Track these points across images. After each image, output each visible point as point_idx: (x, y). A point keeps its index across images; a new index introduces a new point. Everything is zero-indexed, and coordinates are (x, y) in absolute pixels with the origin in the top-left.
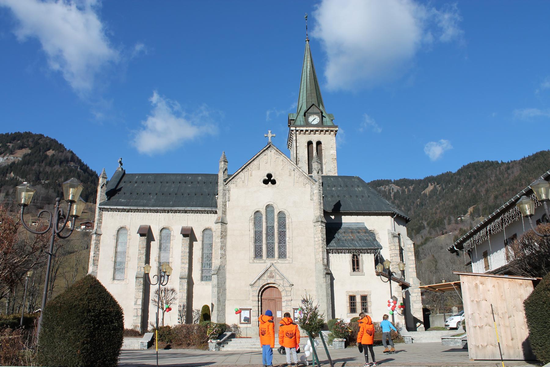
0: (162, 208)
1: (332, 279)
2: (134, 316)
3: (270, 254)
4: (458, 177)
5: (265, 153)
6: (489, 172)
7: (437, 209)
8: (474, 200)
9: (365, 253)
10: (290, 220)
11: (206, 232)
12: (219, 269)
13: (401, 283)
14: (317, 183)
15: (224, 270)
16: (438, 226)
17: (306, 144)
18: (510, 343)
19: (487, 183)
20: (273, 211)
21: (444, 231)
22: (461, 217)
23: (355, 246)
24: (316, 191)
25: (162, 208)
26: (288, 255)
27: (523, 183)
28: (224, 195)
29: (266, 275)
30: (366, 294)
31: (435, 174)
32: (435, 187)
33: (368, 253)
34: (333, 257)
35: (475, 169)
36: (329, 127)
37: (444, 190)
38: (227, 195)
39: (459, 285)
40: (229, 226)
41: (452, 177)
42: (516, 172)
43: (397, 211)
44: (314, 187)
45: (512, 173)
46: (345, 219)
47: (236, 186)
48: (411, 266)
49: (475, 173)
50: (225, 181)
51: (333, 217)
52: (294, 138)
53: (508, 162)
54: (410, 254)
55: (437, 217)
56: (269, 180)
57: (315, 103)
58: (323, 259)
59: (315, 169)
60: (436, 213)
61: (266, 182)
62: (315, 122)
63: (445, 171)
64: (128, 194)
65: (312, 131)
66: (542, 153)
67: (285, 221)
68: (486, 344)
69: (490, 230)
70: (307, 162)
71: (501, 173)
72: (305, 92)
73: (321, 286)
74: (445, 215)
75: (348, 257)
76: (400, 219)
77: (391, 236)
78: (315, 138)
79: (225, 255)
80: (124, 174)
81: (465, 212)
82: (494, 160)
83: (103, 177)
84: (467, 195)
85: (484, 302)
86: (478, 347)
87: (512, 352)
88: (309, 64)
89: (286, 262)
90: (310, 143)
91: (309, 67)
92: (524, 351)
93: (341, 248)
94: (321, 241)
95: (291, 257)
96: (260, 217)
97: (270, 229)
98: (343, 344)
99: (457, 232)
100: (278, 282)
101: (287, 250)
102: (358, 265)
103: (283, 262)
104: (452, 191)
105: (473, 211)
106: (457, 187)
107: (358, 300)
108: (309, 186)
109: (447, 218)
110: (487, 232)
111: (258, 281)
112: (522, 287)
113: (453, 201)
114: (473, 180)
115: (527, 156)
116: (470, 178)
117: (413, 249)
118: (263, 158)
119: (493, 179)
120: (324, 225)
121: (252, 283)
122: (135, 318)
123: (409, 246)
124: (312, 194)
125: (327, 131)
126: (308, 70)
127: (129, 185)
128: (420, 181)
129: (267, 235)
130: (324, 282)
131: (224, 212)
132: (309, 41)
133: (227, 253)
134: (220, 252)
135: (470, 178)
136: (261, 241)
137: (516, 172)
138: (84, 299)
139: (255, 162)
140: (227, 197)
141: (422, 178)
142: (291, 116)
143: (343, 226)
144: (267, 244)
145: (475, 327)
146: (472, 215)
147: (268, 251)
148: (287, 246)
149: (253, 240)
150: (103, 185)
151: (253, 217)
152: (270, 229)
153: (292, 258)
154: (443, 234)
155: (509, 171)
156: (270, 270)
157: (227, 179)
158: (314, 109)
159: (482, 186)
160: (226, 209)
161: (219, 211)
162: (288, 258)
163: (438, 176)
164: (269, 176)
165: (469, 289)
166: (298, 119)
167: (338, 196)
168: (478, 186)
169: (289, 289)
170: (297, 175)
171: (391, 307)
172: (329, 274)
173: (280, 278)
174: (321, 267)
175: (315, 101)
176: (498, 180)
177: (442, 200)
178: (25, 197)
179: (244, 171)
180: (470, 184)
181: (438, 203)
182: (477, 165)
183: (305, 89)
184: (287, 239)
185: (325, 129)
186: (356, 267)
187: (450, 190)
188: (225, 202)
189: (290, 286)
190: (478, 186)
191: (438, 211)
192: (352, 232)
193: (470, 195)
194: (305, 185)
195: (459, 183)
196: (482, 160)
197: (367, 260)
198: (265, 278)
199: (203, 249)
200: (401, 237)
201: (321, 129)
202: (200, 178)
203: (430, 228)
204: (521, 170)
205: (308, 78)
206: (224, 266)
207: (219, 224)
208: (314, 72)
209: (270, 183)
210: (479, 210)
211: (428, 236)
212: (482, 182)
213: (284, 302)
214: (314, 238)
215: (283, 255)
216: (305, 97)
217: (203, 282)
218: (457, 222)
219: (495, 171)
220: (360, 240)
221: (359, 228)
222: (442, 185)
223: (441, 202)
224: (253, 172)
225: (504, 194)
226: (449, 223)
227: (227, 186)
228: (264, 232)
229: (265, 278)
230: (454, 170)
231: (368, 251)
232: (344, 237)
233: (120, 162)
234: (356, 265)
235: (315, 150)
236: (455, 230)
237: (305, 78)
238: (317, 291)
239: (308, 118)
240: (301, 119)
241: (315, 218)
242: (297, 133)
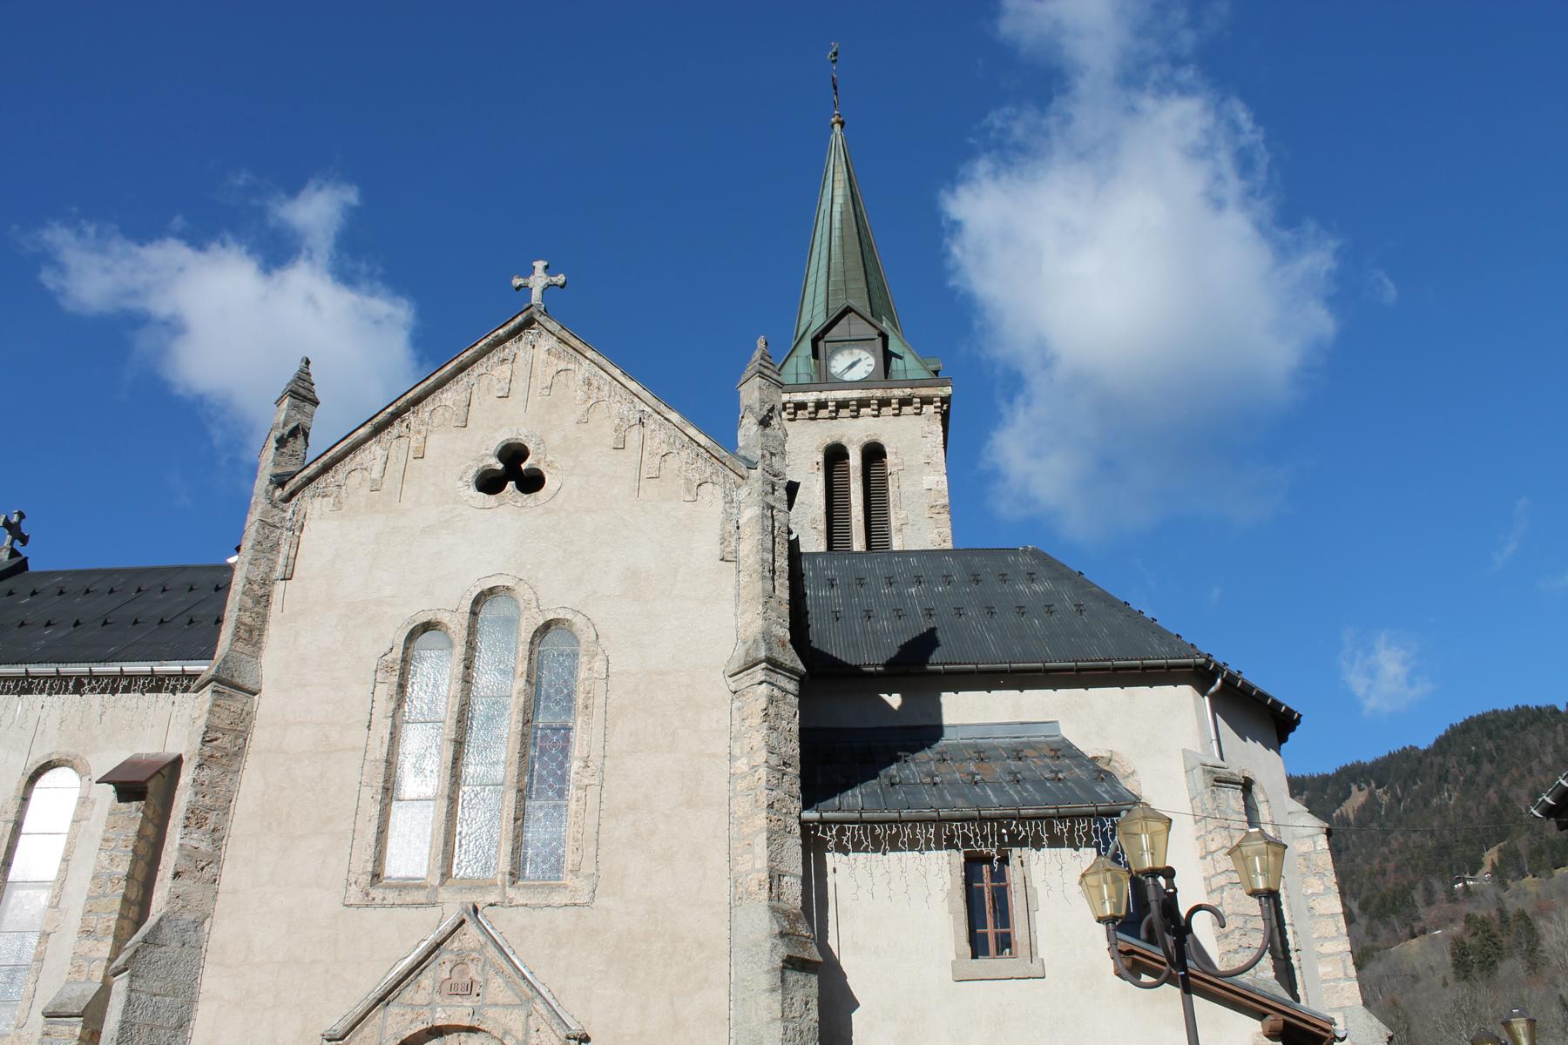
4: (1439, 759)
5: (498, 354)
6: (1533, 740)
7: (1386, 860)
8: (1500, 825)
9: (1037, 845)
10: (599, 665)
13: (1276, 1020)
14: (756, 474)
16: (1394, 911)
17: (820, 458)
19: (1530, 772)
21: (1417, 926)
29: (426, 980)
31: (1367, 758)
32: (1371, 794)
33: (1056, 842)
34: (847, 873)
35: (1490, 735)
36: (913, 384)
37: (1399, 801)
38: (284, 549)
40: (265, 706)
41: (1420, 761)
46: (963, 710)
47: (338, 504)
48: (1329, 947)
49: (1489, 745)
50: (280, 481)
51: (895, 700)
54: (1315, 885)
55: (1390, 885)
57: (853, 303)
58: (775, 877)
59: (750, 408)
60: (1383, 872)
61: (489, 483)
63: (1396, 747)
65: (842, 405)
70: (822, 526)
74: (1411, 876)
75: (935, 874)
77: (1200, 780)
78: (854, 433)
81: (1475, 866)
82: (1542, 704)
84: (1473, 814)
89: (557, 899)
90: (835, 456)
91: (839, 200)
94: (763, 772)
95: (588, 868)
99: (1457, 929)
104: (1426, 803)
105: (1500, 860)
106: (1439, 791)
108: (718, 491)
109: (1420, 886)
111: (378, 1016)
113: (1432, 833)
114: (1487, 768)
116: (1475, 760)
117: (1326, 860)
118: (491, 375)
119: (1549, 760)
120: (792, 686)
121: (340, 1028)
123: (1305, 846)
125: (904, 402)
126: (837, 208)
128: (1325, 779)
132: (842, 124)
135: (1475, 760)
140: (281, 560)
141: (1330, 771)
153: (595, 877)
154: (1414, 936)
156: (454, 945)
160: (264, 619)
162: (568, 880)
163: (1376, 763)
167: (929, 613)
168: (1506, 782)
173: (507, 996)
174: (759, 924)
177: (1397, 834)
179: (384, 436)
180: (1479, 779)
181: (1385, 842)
182: (1493, 721)
184: (575, 766)
185: (898, 393)
188: (266, 582)
190: (1506, 782)
191: (1390, 866)
193: (1483, 809)
195: (1443, 778)
196: (1506, 704)
200: (1259, 796)
203: (1372, 918)
206: (198, 924)
208: (858, 216)
209: (511, 485)
211: (1368, 943)
212: (1514, 771)
214: (732, 758)
218: (1452, 897)
219: (1551, 735)
222: (1391, 788)
223: (1396, 840)
224: (433, 440)
226: (1429, 902)
230: (1425, 742)
231: (1058, 828)
234: (988, 925)
236: (1452, 921)
239: (828, 359)
241: (741, 651)
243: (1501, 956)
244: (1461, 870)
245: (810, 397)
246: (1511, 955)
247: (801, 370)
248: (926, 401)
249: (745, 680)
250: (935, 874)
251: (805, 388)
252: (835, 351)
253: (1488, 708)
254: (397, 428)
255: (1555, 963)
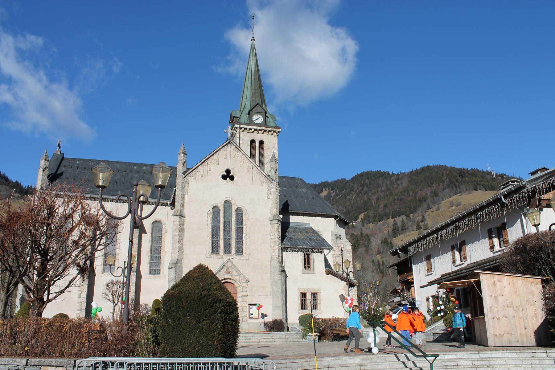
0: (111, 197)
1: (286, 276)
2: (78, 310)
3: (227, 250)
4: (352, 184)
6: (381, 182)
8: (365, 207)
11: (156, 225)
12: (177, 263)
14: (274, 182)
15: (181, 264)
17: (249, 143)
18: (524, 332)
19: (378, 192)
20: (230, 207)
22: (353, 223)
23: (308, 245)
24: (273, 190)
25: (111, 197)
26: (244, 251)
27: (411, 194)
28: (183, 188)
29: (222, 271)
30: (316, 291)
31: (330, 180)
32: (329, 192)
33: (319, 252)
35: (368, 178)
36: (272, 127)
39: (478, 283)
40: (187, 219)
41: (346, 184)
42: (405, 183)
43: (338, 213)
44: (271, 185)
45: (401, 184)
47: (195, 179)
49: (367, 182)
50: (184, 173)
52: (238, 135)
53: (398, 174)
54: (348, 255)
56: (228, 176)
58: (279, 256)
61: (224, 177)
62: (259, 122)
63: (339, 178)
64: (71, 179)
66: (428, 168)
67: (242, 217)
68: (503, 333)
69: (441, 236)
71: (391, 183)
72: (249, 90)
73: (276, 283)
75: (300, 256)
76: (342, 223)
78: (258, 137)
79: (182, 249)
80: (63, 158)
81: (356, 219)
82: (385, 171)
83: (45, 160)
84: (359, 202)
85: (501, 297)
86: (496, 335)
87: (525, 340)
88: (254, 63)
89: (243, 258)
90: (253, 142)
91: (254, 66)
92: (535, 338)
93: (295, 247)
94: (277, 239)
95: (248, 253)
96: (218, 212)
97: (228, 224)
98: (317, 338)
100: (234, 277)
101: (244, 247)
102: (309, 264)
103: (240, 258)
104: (346, 197)
106: (350, 194)
107: (309, 297)
110: (437, 238)
112: (533, 284)
113: (346, 207)
114: (366, 189)
115: (415, 169)
116: (363, 186)
118: (222, 154)
119: (384, 188)
122: (79, 312)
124: (269, 193)
125: (270, 131)
126: (253, 69)
127: (70, 170)
129: (225, 230)
130: (278, 278)
131: (182, 205)
133: (184, 247)
134: (177, 246)
135: (363, 186)
136: (218, 236)
137: (405, 183)
138: (538, 269)
139: (215, 157)
140: (185, 190)
141: (318, 183)
142: (234, 113)
143: (291, 225)
144: (225, 239)
145: (494, 318)
146: (363, 221)
147: (225, 247)
148: (244, 242)
149: (210, 236)
150: (45, 168)
151: (211, 211)
152: (228, 224)
155: (399, 182)
157: (186, 172)
158: (258, 108)
159: (373, 194)
161: (177, 205)
162: (244, 255)
164: (228, 171)
165: (488, 286)
166: (242, 117)
168: (370, 194)
169: (245, 285)
170: (255, 173)
171: (349, 304)
172: (284, 271)
173: (236, 274)
174: (277, 264)
175: (258, 101)
176: (389, 189)
178: (103, 178)
180: (363, 192)
183: (249, 88)
184: (244, 235)
185: (269, 129)
186: (307, 265)
187: (344, 196)
189: (246, 282)
190: (370, 194)
192: (300, 232)
193: (362, 202)
194: (262, 183)
195: (352, 190)
196: (375, 170)
197: (317, 259)
198: (222, 274)
199: (152, 241)
201: (264, 128)
202: (145, 168)
204: (409, 182)
205: (253, 77)
207: (178, 217)
209: (228, 178)
210: (369, 216)
212: (373, 191)
213: (240, 297)
215: (239, 251)
216: (249, 96)
217: (151, 276)
220: (310, 239)
221: (306, 228)
222: (336, 191)
224: (212, 167)
225: (393, 203)
227: (188, 177)
228: (222, 227)
229: (222, 274)
230: (348, 177)
231: (320, 251)
232: (294, 236)
233: (59, 145)
234: (307, 263)
235: (257, 150)
237: (250, 77)
238: (272, 288)
239: (252, 116)
240: (244, 117)
241: (272, 216)
242: (241, 130)
243: (359, 247)
244: (352, 219)
245: (248, 127)
246: (362, 247)
247: (245, 118)
248: (275, 132)
249: (273, 222)
250: (300, 256)
251: (247, 124)
252: (254, 114)
253: (369, 170)
254: (205, 164)
255: (373, 250)
